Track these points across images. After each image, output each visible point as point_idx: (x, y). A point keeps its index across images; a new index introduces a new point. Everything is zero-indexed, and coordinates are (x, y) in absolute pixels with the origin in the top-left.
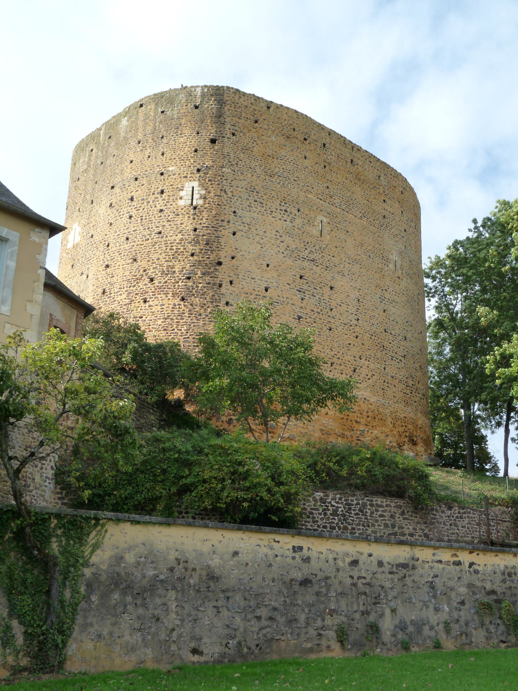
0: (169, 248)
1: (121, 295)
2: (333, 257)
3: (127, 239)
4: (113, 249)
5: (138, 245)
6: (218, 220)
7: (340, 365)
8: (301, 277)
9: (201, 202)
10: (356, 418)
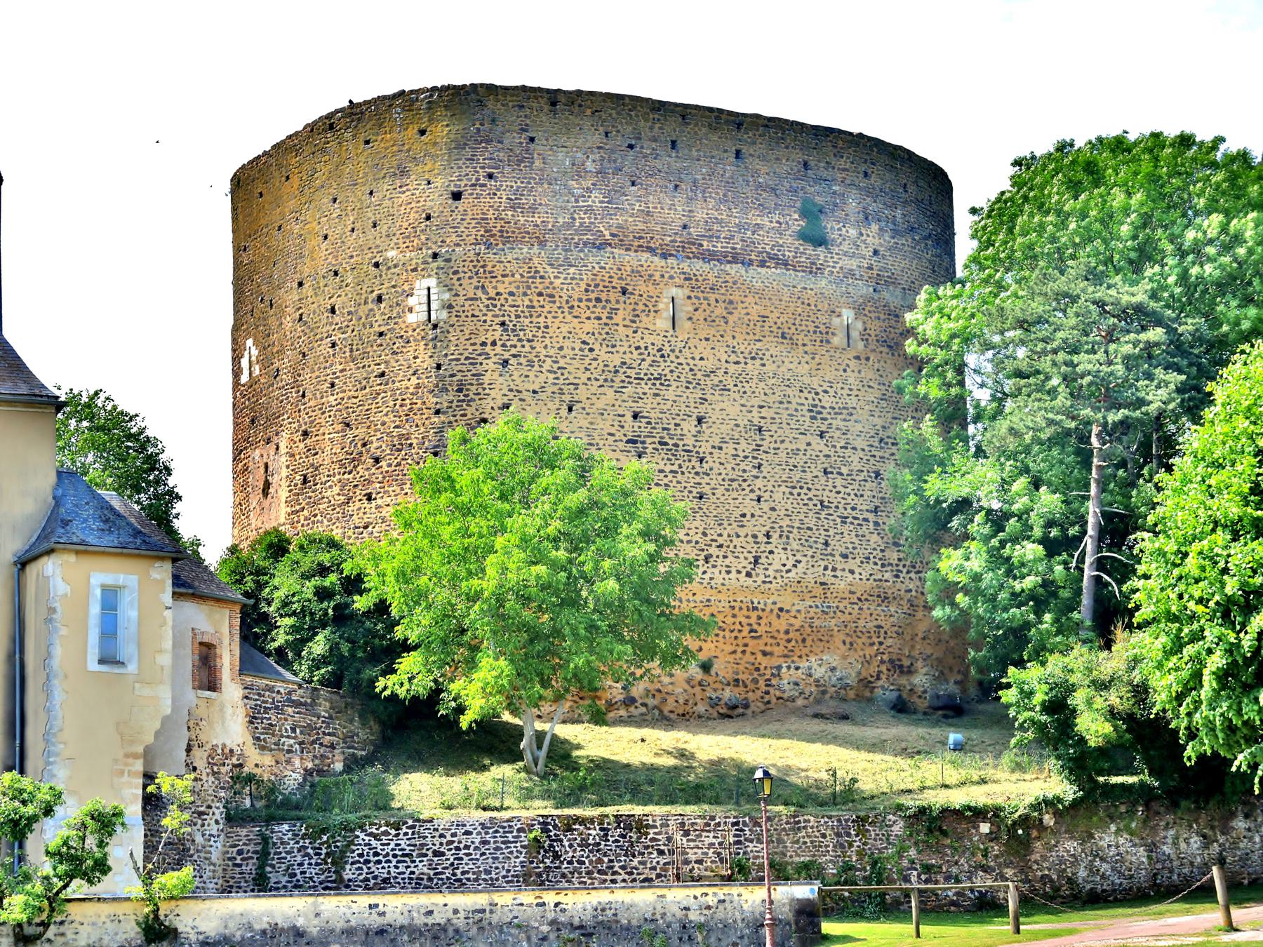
0: (399, 402)
1: (331, 487)
2: (702, 359)
3: (333, 385)
4: (311, 403)
5: (349, 398)
6: (475, 344)
7: (725, 557)
8: (635, 416)
9: (444, 315)
10: (763, 648)
